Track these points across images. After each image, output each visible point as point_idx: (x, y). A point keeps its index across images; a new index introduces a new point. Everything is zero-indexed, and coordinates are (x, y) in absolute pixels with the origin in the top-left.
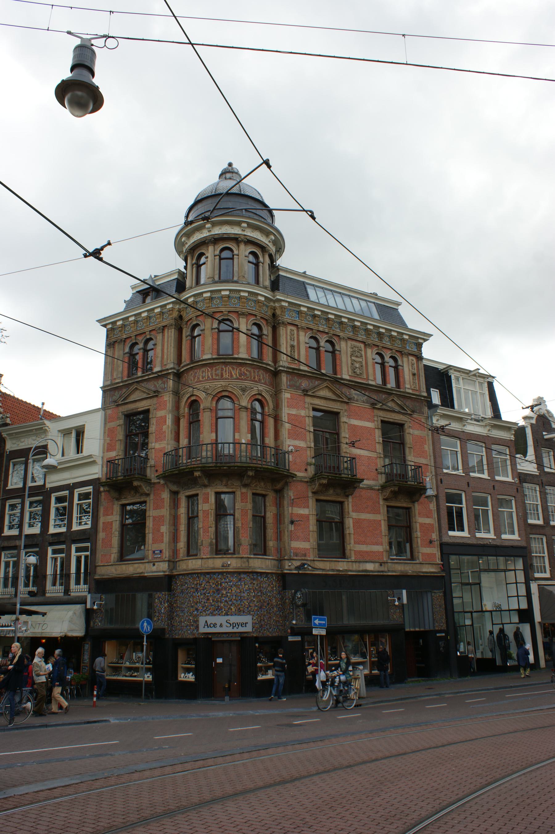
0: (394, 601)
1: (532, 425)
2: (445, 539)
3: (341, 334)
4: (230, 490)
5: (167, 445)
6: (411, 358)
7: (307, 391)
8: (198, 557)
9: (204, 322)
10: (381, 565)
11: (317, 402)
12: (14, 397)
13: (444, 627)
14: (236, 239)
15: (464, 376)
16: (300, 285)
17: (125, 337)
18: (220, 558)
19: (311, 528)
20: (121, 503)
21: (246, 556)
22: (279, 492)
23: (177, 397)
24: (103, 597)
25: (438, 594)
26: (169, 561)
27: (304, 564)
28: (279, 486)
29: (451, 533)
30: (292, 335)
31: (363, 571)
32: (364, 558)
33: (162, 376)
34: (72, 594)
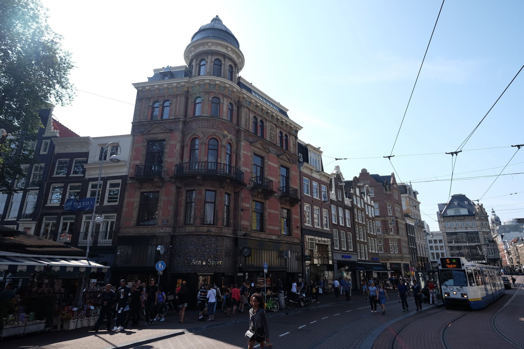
4: (214, 189)
5: (176, 160)
12: (58, 122)
17: (150, 96)
20: (141, 191)
28: (237, 191)
30: (247, 113)
32: (272, 232)
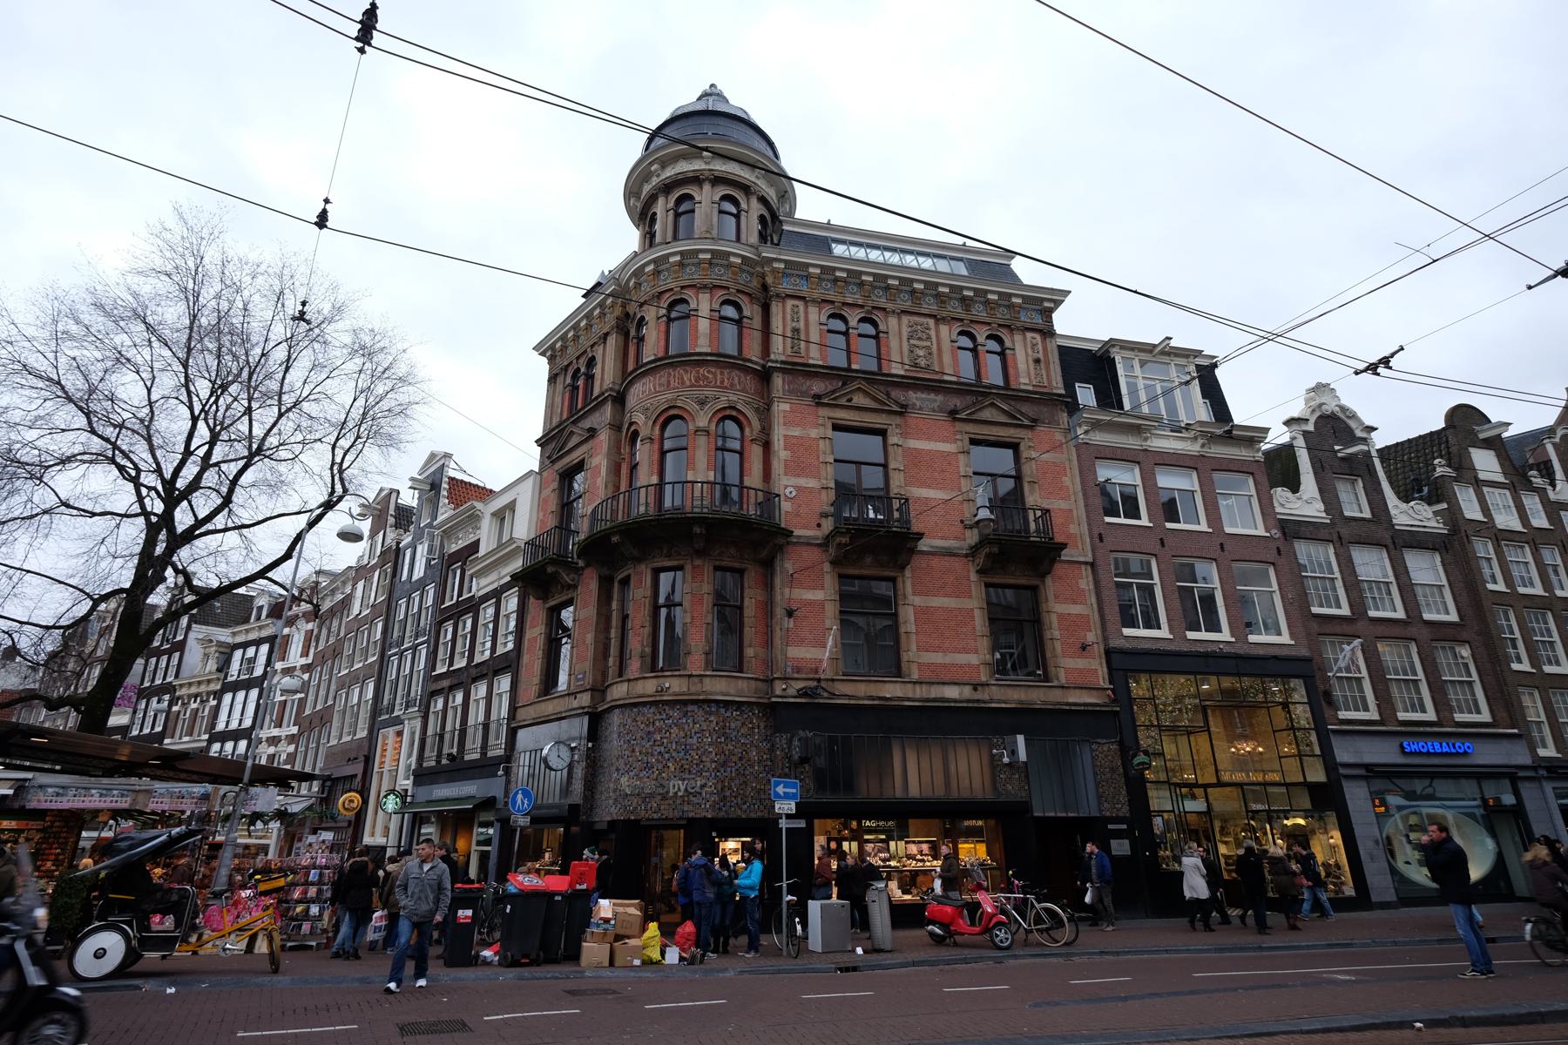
0: (1002, 755)
1: (1305, 434)
2: (1115, 643)
3: (889, 306)
4: (675, 563)
6: (1029, 335)
10: (975, 689)
13: (1125, 811)
14: (696, 179)
15: (1144, 356)
16: (820, 239)
22: (768, 565)
25: (1107, 749)
28: (764, 553)
29: (1127, 631)
31: (935, 700)
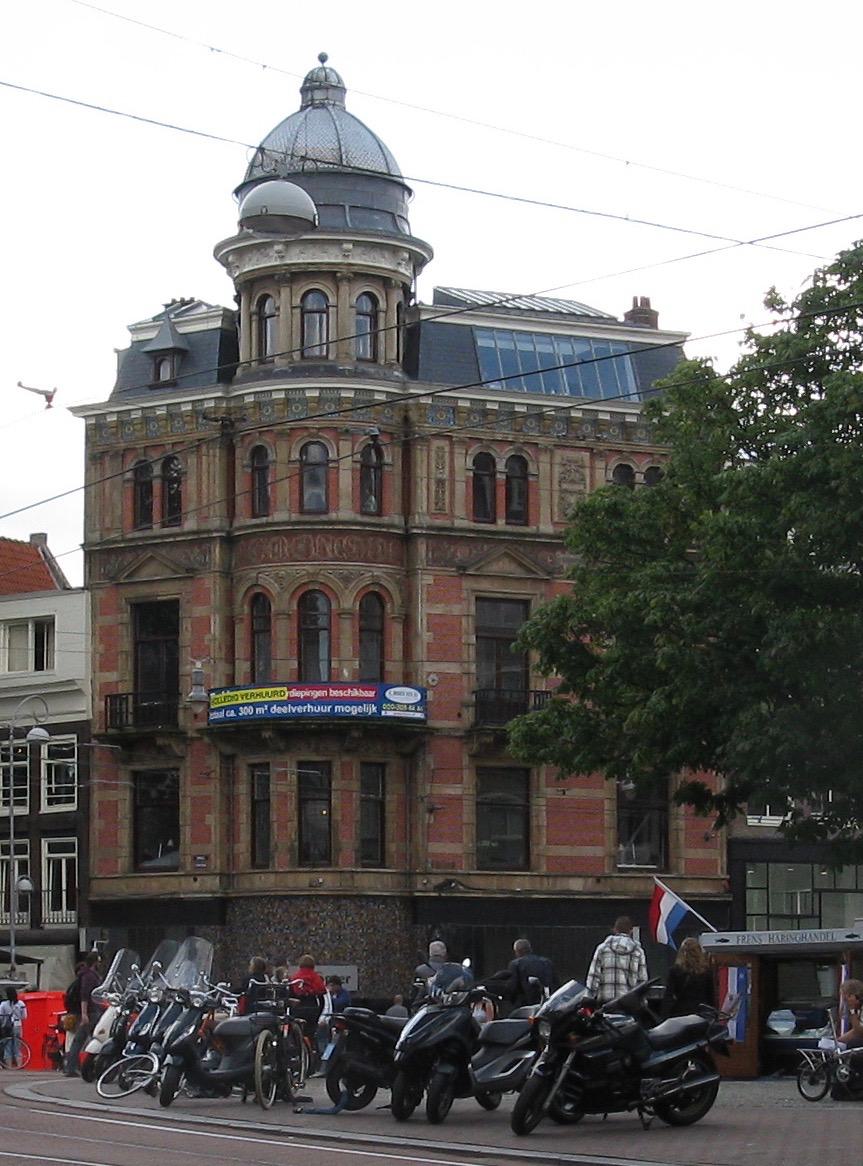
3: (541, 441)
7: (465, 569)
8: (270, 870)
9: (275, 445)
10: (598, 881)
11: (486, 586)
14: (331, 274)
17: (123, 445)
18: (306, 872)
19: (465, 819)
20: (131, 768)
21: (349, 869)
23: (229, 581)
24: (106, 932)
26: (221, 875)
27: (451, 882)
28: (408, 749)
32: (566, 868)
33: (200, 540)
34: (47, 927)
